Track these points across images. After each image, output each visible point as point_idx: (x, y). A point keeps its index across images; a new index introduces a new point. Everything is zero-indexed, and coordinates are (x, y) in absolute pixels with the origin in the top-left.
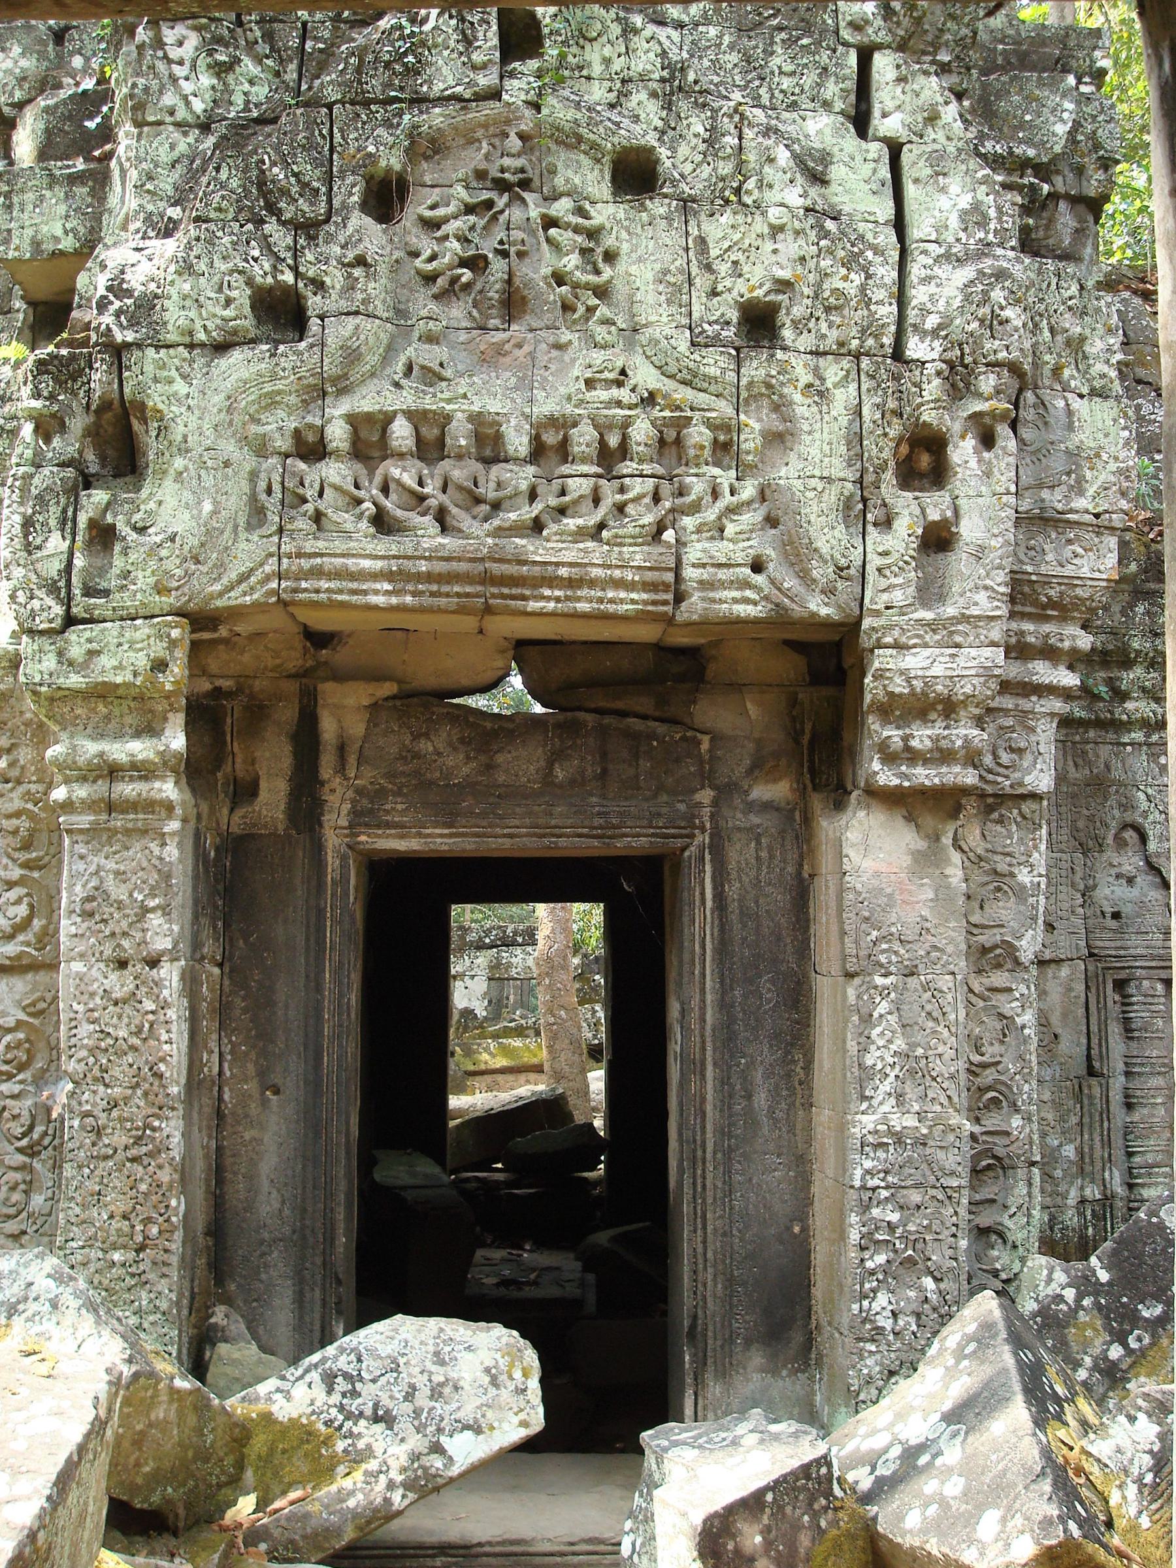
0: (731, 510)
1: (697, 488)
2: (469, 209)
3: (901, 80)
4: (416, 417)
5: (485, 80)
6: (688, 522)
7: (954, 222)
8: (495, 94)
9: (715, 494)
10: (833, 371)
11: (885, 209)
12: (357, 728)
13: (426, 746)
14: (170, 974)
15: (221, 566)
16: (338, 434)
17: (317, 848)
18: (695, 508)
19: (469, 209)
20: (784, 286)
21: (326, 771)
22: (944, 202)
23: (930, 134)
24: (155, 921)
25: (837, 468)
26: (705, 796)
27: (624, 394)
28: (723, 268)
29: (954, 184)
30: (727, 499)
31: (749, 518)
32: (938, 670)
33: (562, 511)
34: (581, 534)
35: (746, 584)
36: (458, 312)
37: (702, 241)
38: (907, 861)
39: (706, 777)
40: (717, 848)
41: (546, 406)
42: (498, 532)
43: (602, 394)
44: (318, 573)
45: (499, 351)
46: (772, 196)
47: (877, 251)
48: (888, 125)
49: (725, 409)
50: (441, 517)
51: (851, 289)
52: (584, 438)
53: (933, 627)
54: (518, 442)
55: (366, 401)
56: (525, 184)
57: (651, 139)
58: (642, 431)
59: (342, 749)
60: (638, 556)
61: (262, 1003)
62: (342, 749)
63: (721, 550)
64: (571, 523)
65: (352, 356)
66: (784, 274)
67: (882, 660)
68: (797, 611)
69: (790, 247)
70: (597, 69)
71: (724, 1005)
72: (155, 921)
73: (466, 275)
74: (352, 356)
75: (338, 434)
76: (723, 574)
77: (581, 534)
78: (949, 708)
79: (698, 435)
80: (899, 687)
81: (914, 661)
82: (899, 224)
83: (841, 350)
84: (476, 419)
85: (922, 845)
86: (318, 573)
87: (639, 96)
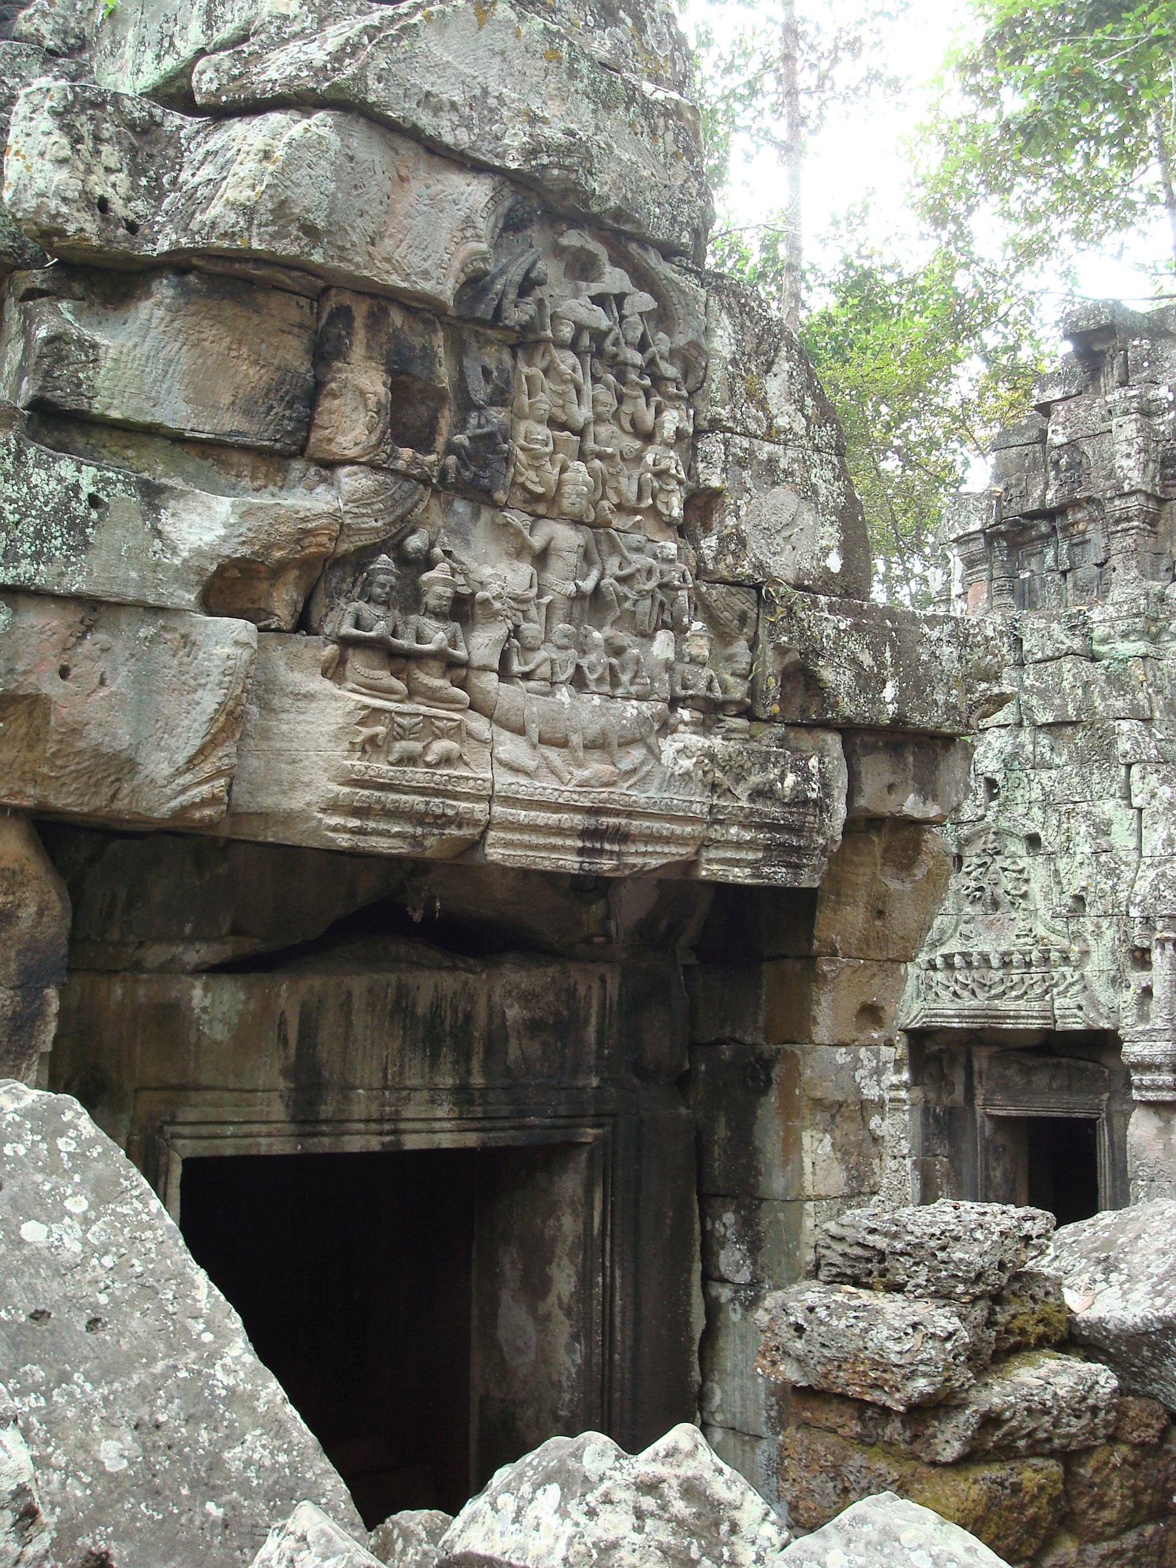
0: (1072, 984)
1: (1056, 976)
2: (980, 866)
3: (1143, 778)
4: (962, 954)
5: (980, 812)
6: (1055, 990)
7: (1160, 846)
8: (983, 818)
9: (1064, 977)
10: (1105, 923)
11: (1132, 843)
12: (985, 1065)
13: (1007, 1072)
14: (908, 1162)
15: (908, 1013)
16: (939, 962)
17: (974, 1113)
18: (1056, 985)
19: (980, 866)
20: (1084, 889)
21: (976, 1083)
22: (1156, 837)
23: (1153, 802)
24: (903, 1142)
25: (1106, 965)
26: (1105, 1096)
27: (1029, 940)
28: (1065, 881)
29: (1160, 827)
30: (1069, 980)
31: (1077, 988)
32: (1146, 1052)
33: (1012, 988)
34: (1017, 998)
35: (1076, 1016)
36: (979, 908)
37: (1056, 871)
38: (1155, 1131)
39: (1107, 1088)
40: (1109, 1119)
41: (1004, 948)
42: (989, 999)
43: (1022, 940)
44: (936, 1016)
45: (992, 923)
46: (1079, 850)
47: (1127, 864)
48: (1137, 802)
49: (1065, 942)
50: (973, 993)
51: (1107, 888)
52: (1016, 957)
53: (1143, 1033)
54: (995, 963)
55: (945, 950)
56: (998, 853)
57: (1038, 830)
58: (1035, 955)
59: (980, 1073)
60: (1036, 1005)
61: (959, 1173)
62: (980, 1073)
63: (1066, 1002)
64: (1014, 993)
65: (942, 932)
66: (1084, 884)
67: (1126, 1047)
68: (1096, 1027)
69: (1087, 870)
70: (1020, 800)
71: (1114, 1187)
72: (903, 1142)
73: (978, 894)
74: (942, 932)
75: (939, 962)
76: (1067, 1012)
77: (1017, 998)
78: (1158, 1068)
79: (1054, 955)
80: (1132, 1059)
81: (1136, 1048)
82: (1139, 849)
83: (1105, 915)
84: (980, 953)
85: (1161, 1124)
86: (936, 1016)
87: (1035, 809)
